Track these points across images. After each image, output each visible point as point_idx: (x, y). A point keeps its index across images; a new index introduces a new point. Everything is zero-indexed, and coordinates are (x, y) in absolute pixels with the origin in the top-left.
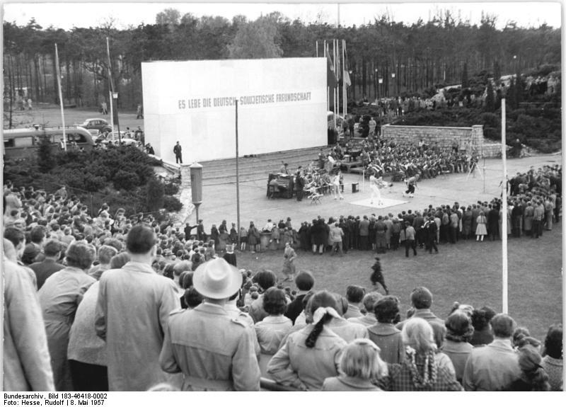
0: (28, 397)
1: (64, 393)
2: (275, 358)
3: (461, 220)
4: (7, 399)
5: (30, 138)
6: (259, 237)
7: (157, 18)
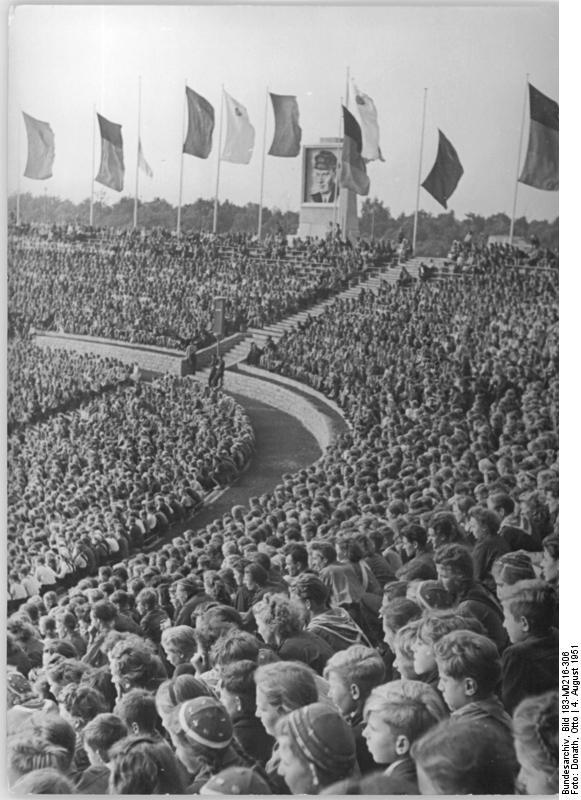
0: (567, 761)
1: (561, 709)
2: (144, 595)
3: (238, 583)
4: (570, 790)
5: (222, 162)
6: (546, 415)
7: (50, 780)
